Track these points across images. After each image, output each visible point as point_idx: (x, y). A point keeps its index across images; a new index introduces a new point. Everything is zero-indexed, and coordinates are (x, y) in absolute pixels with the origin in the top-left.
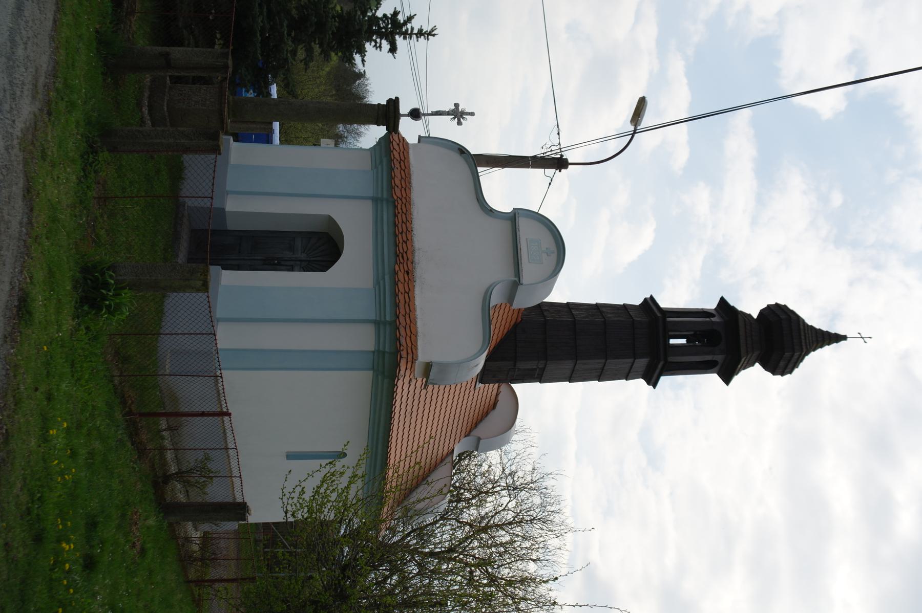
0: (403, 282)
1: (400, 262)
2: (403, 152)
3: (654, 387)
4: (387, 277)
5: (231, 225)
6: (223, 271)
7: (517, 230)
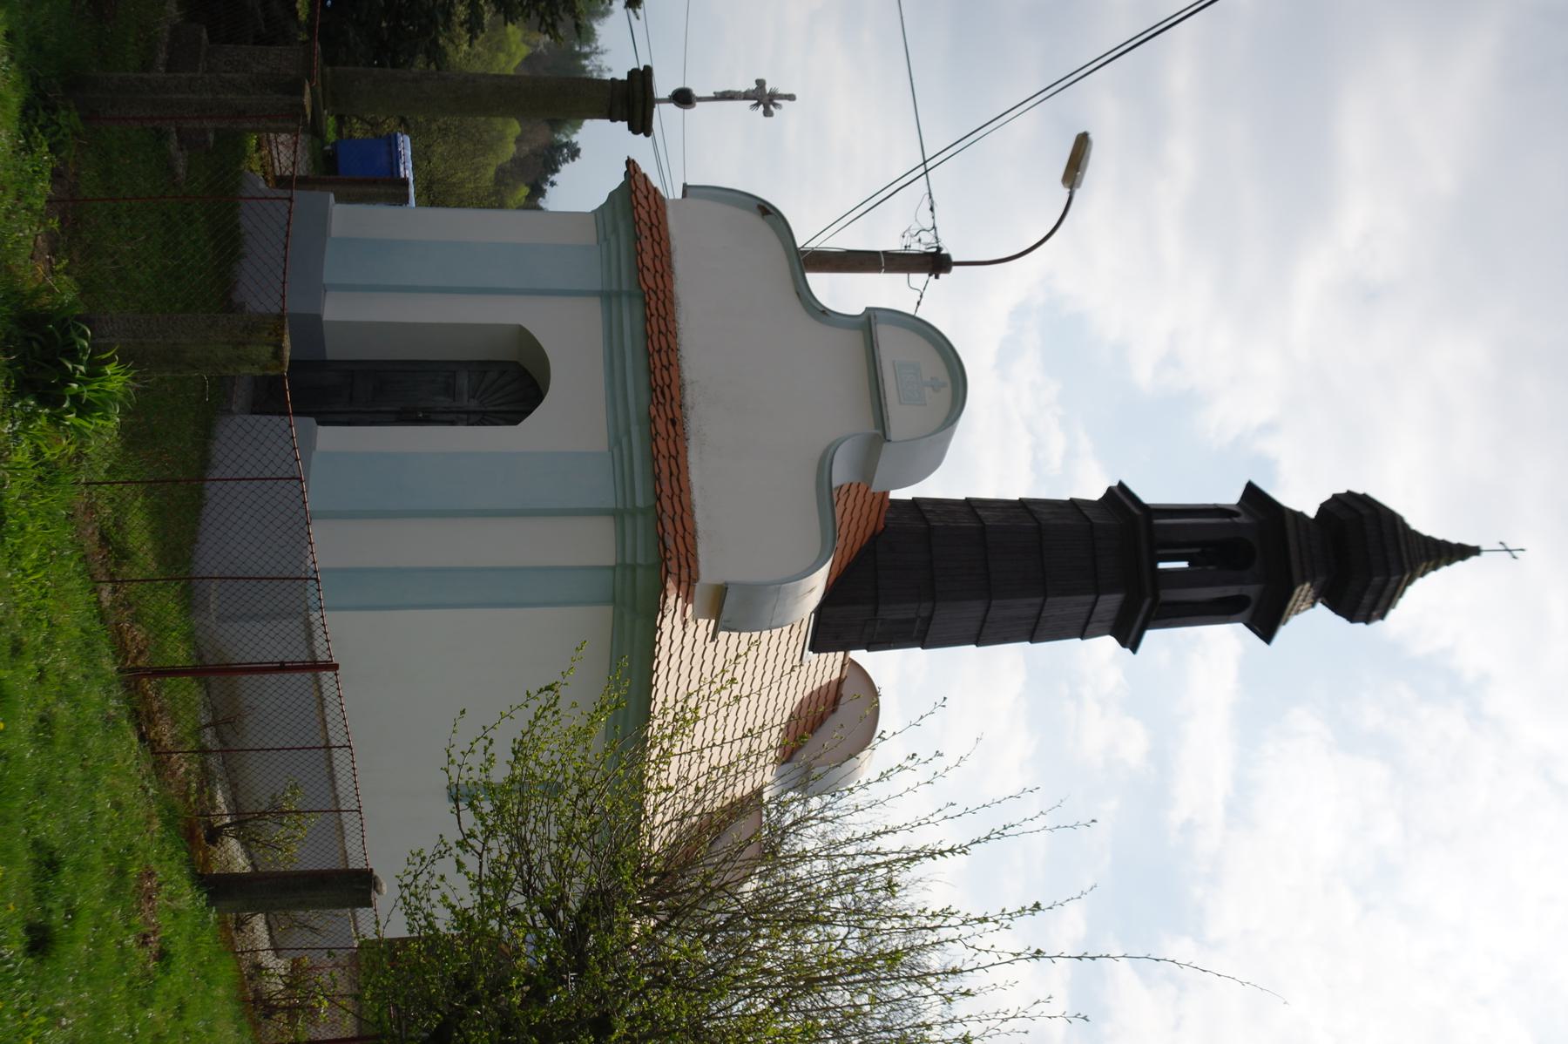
0: (666, 437)
1: (658, 402)
2: (656, 212)
3: (1134, 649)
4: (635, 430)
5: (334, 351)
6: (320, 428)
7: (875, 345)
